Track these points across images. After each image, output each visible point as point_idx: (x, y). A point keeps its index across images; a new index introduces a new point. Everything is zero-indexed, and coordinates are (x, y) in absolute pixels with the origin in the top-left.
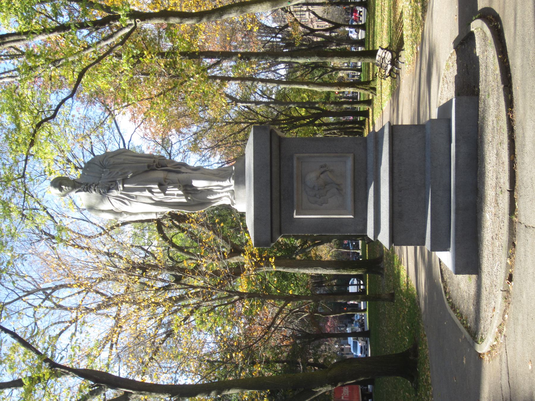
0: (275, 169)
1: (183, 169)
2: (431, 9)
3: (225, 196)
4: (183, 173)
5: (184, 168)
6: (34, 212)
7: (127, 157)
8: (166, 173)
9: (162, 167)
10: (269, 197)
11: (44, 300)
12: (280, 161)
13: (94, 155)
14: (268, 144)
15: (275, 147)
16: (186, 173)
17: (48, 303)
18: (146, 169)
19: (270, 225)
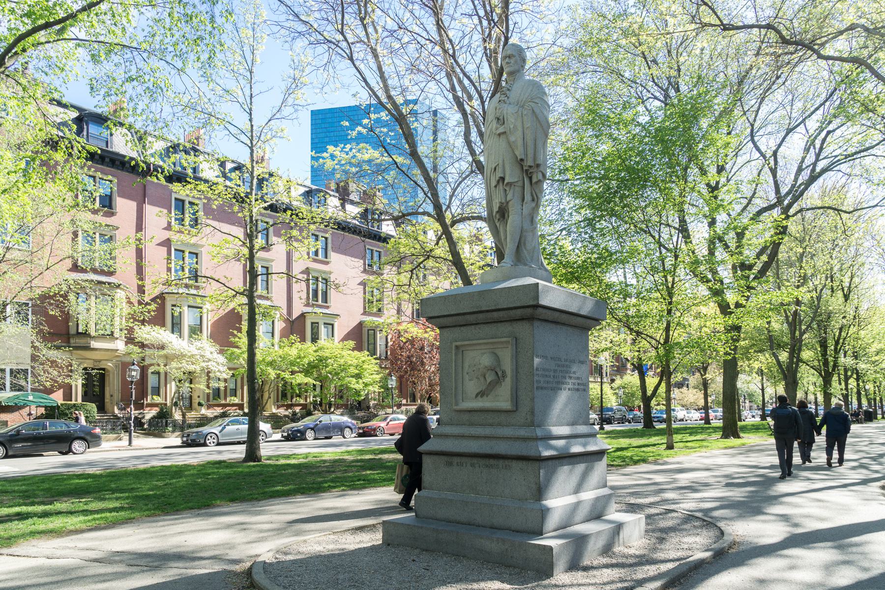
0: (495, 315)
1: (528, 206)
8: (520, 184)
14: (519, 305)
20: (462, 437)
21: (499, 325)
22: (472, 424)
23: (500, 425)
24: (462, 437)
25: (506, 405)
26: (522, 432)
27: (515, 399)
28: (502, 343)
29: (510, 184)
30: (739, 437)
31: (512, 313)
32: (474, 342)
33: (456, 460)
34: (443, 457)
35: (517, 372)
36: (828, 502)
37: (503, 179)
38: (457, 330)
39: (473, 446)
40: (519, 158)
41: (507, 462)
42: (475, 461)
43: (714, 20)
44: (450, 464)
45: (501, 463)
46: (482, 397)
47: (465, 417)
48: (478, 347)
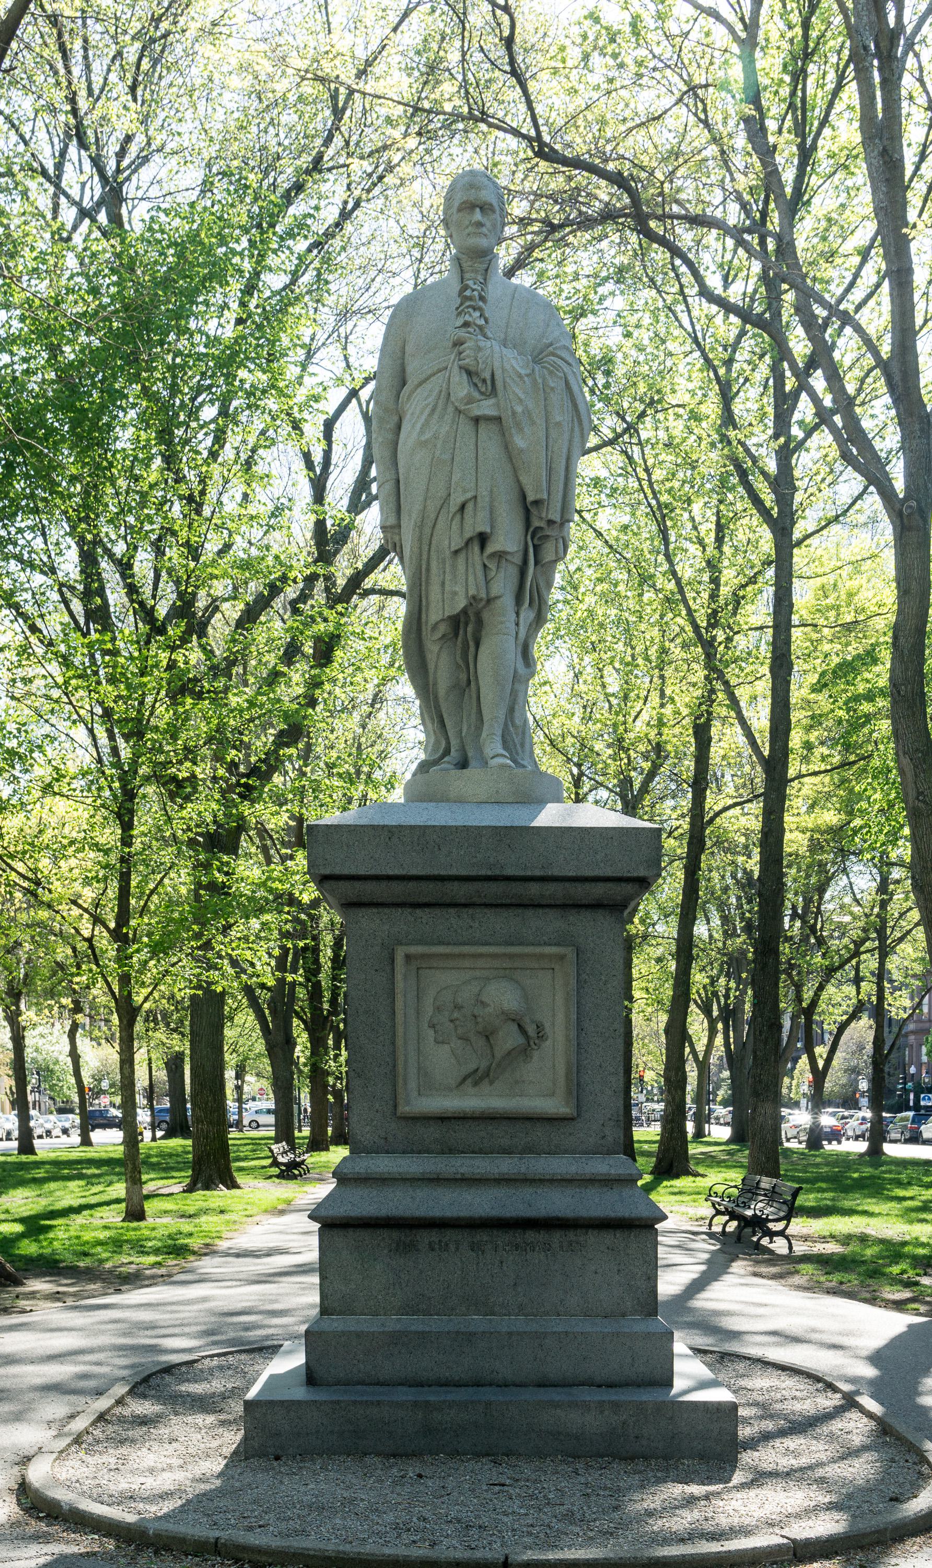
0: (534, 889)
1: (527, 615)
2: (11, 1554)
3: (448, 743)
4: (518, 614)
5: (532, 615)
6: (713, 349)
7: (566, 436)
8: (518, 559)
9: (536, 547)
10: (453, 872)
11: (78, 204)
12: (540, 906)
13: (866, 488)
14: (609, 872)
15: (598, 891)
16: (517, 624)
17: (68, 214)
18: (531, 498)
19: (372, 872)
20: (436, 1180)
21: (530, 913)
22: (450, 1150)
23: (530, 1150)
24: (436, 1180)
25: (554, 1105)
26: (601, 1166)
27: (577, 1089)
28: (542, 956)
29: (500, 556)
30: (237, 1186)
31: (579, 891)
32: (466, 949)
33: (425, 1237)
34: (385, 1233)
35: (580, 1029)
36: (773, 1306)
37: (483, 539)
38: (405, 914)
39: (480, 1203)
40: (531, 498)
41: (571, 1235)
42: (482, 1236)
43: (518, 117)
44: (406, 1248)
45: (557, 1237)
46: (476, 1084)
47: (432, 1132)
48: (467, 963)
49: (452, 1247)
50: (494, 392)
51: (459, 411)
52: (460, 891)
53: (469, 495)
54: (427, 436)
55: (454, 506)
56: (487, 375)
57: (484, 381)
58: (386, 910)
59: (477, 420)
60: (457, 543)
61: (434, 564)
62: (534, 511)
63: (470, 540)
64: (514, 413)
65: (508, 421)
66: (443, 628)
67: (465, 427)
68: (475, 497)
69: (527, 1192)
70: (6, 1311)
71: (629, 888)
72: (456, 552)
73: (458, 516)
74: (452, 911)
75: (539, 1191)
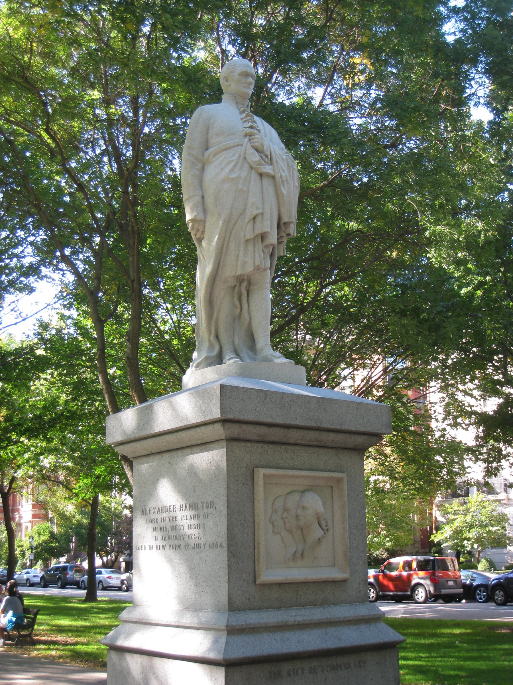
21: (321, 451)
33: (286, 667)
49: (300, 671)
50: (271, 163)
51: (252, 168)
52: (294, 435)
53: (260, 211)
54: (233, 176)
55: (249, 215)
56: (269, 153)
57: (267, 156)
58: (249, 445)
59: (261, 175)
60: (249, 235)
61: (232, 245)
62: (283, 228)
63: (257, 235)
64: (281, 176)
65: (278, 178)
66: (232, 282)
67: (254, 176)
68: (262, 214)
69: (332, 631)
70: (487, 636)
71: (360, 440)
72: (247, 241)
73: (252, 222)
74: (283, 447)
75: (338, 629)
